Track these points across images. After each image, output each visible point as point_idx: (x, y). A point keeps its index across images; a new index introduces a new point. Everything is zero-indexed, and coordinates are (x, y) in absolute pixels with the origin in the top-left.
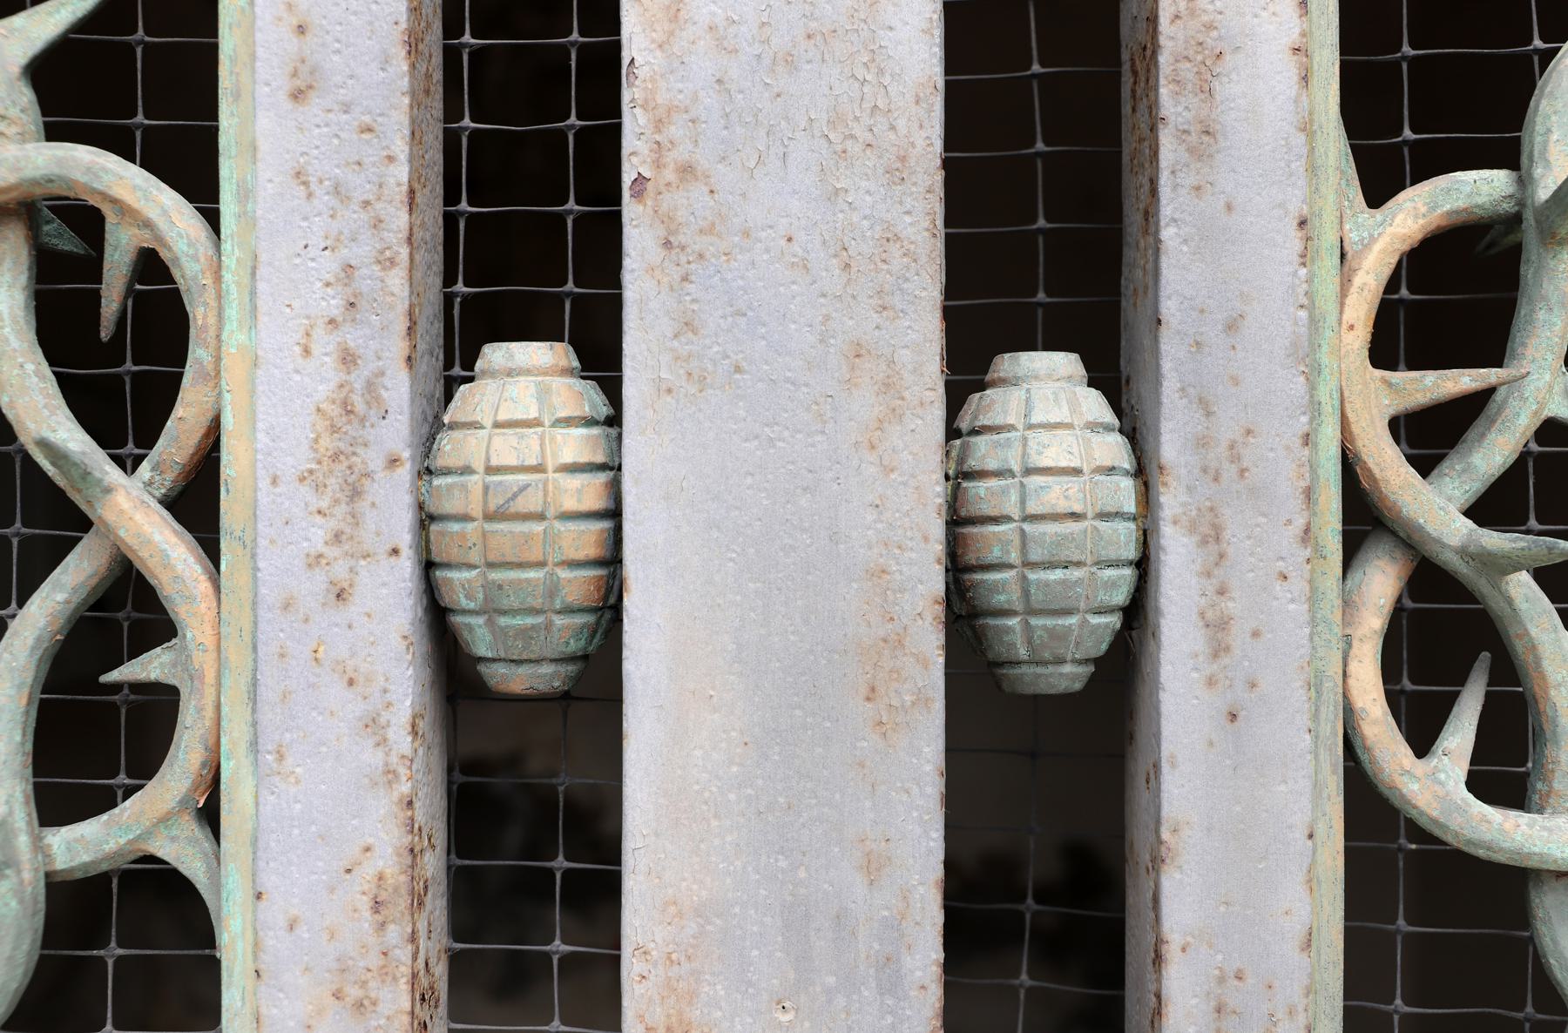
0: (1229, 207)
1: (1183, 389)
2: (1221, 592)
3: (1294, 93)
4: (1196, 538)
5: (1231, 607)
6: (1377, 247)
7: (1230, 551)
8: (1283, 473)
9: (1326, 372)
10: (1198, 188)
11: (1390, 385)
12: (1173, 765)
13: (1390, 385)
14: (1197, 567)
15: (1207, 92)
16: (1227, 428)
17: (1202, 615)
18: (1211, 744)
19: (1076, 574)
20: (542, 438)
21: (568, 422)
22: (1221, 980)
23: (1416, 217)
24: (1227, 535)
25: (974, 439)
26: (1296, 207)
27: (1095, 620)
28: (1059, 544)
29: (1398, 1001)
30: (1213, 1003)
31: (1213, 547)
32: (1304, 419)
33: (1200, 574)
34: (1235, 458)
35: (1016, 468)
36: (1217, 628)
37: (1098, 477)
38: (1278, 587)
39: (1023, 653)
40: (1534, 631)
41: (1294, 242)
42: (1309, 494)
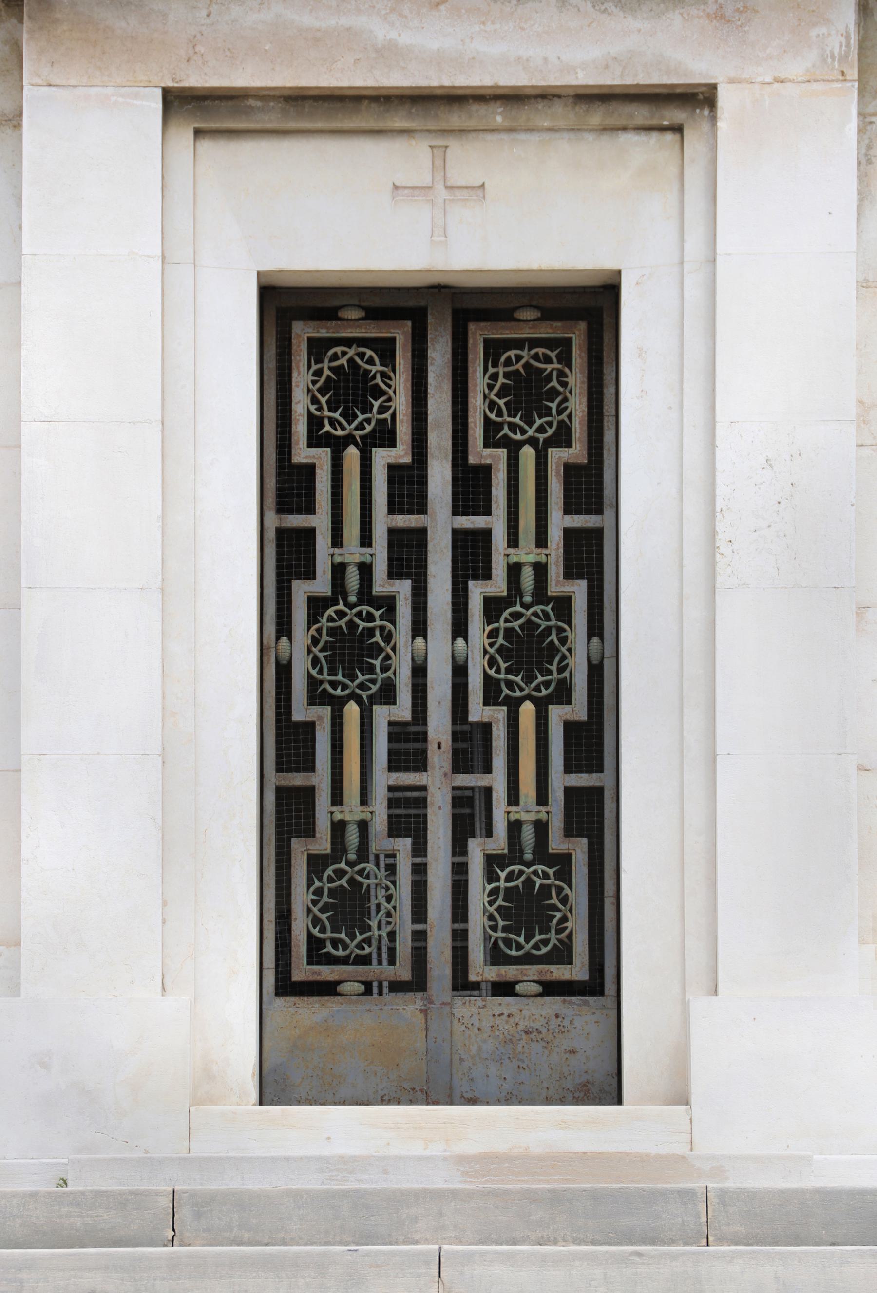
8: (478, 646)
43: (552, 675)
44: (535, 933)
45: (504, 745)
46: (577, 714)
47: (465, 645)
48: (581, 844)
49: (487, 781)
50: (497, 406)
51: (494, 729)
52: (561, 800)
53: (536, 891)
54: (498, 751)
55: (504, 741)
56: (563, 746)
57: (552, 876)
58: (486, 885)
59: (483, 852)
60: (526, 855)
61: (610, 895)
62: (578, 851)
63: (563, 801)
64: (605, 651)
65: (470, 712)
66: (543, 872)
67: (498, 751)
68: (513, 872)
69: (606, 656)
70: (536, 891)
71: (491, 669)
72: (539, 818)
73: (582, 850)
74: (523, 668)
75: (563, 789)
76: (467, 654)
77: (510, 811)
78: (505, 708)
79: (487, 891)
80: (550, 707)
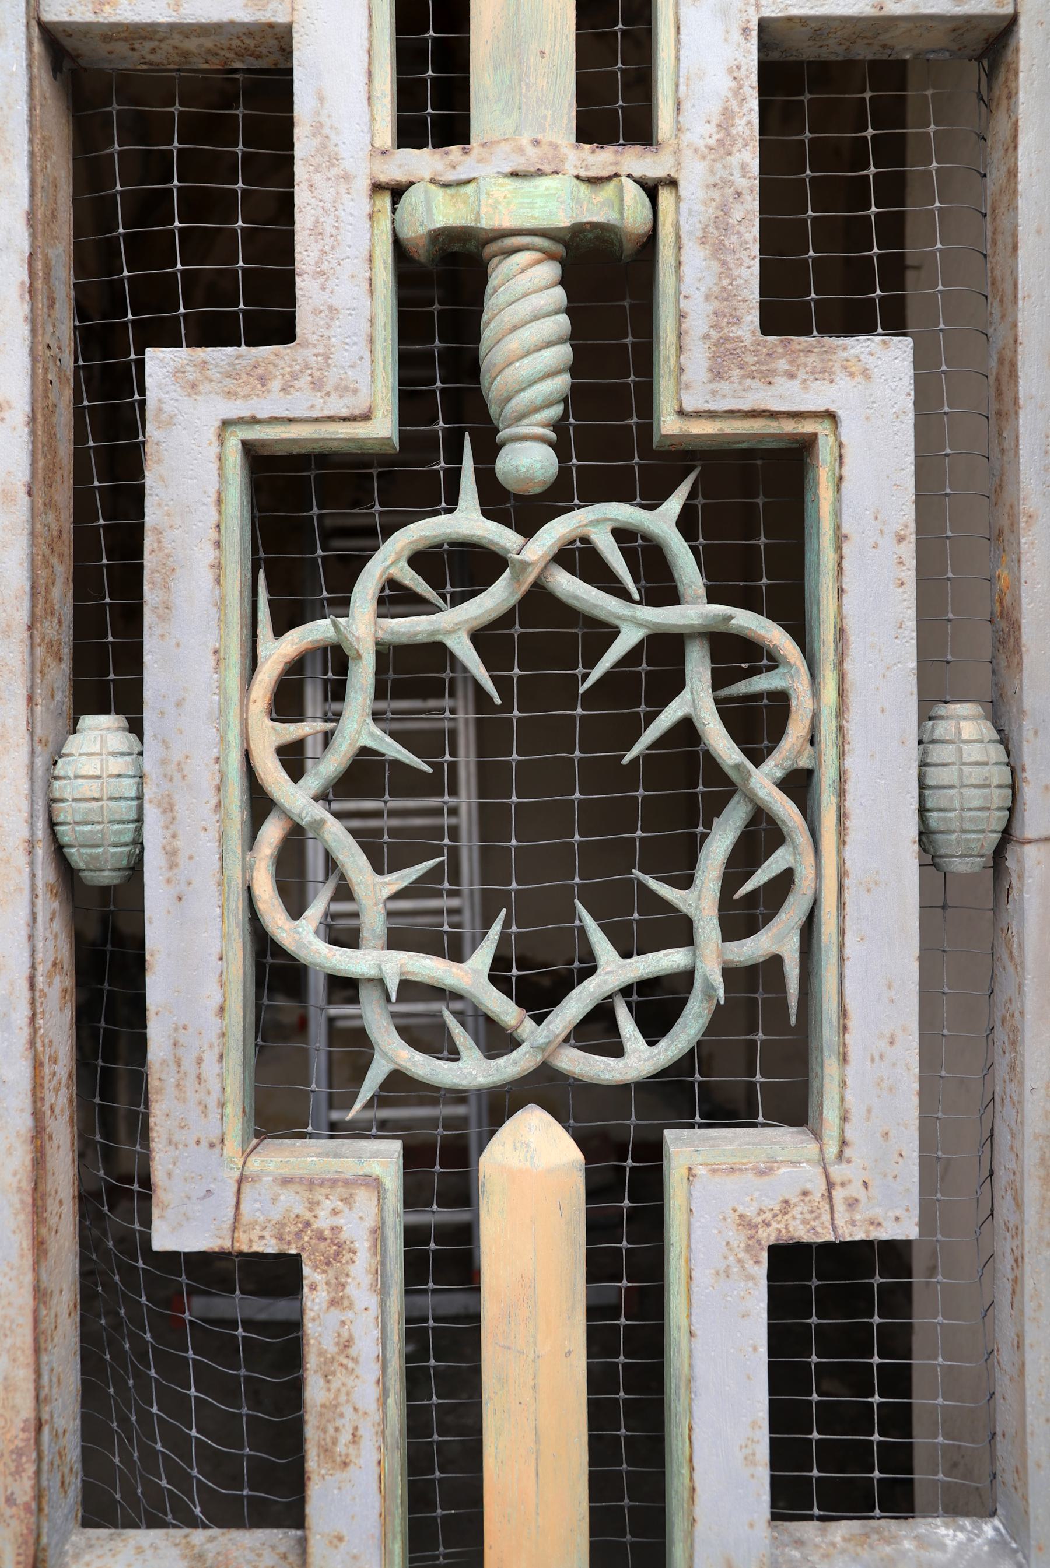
0: (178, 645)
1: (155, 736)
2: (174, 836)
3: (210, 587)
4: (160, 810)
5: (179, 843)
6: (270, 661)
7: (178, 816)
8: (204, 777)
9: (232, 725)
10: (162, 636)
11: (274, 729)
12: (150, 923)
13: (274, 729)
14: (162, 824)
15: (166, 587)
16: (177, 756)
17: (164, 848)
18: (169, 912)
19: (98, 827)
20: (102, 760)
21: (113, 754)
22: (176, 1029)
23: (292, 644)
24: (176, 808)
25: (931, 746)
26: (214, 644)
27: (991, 835)
28: (87, 813)
30: (172, 1041)
31: (169, 814)
32: (215, 750)
33: (163, 828)
34: (180, 770)
35: (72, 775)
36: (171, 854)
37: (111, 780)
38: (202, 834)
41: (211, 661)
46: (852, 1204)
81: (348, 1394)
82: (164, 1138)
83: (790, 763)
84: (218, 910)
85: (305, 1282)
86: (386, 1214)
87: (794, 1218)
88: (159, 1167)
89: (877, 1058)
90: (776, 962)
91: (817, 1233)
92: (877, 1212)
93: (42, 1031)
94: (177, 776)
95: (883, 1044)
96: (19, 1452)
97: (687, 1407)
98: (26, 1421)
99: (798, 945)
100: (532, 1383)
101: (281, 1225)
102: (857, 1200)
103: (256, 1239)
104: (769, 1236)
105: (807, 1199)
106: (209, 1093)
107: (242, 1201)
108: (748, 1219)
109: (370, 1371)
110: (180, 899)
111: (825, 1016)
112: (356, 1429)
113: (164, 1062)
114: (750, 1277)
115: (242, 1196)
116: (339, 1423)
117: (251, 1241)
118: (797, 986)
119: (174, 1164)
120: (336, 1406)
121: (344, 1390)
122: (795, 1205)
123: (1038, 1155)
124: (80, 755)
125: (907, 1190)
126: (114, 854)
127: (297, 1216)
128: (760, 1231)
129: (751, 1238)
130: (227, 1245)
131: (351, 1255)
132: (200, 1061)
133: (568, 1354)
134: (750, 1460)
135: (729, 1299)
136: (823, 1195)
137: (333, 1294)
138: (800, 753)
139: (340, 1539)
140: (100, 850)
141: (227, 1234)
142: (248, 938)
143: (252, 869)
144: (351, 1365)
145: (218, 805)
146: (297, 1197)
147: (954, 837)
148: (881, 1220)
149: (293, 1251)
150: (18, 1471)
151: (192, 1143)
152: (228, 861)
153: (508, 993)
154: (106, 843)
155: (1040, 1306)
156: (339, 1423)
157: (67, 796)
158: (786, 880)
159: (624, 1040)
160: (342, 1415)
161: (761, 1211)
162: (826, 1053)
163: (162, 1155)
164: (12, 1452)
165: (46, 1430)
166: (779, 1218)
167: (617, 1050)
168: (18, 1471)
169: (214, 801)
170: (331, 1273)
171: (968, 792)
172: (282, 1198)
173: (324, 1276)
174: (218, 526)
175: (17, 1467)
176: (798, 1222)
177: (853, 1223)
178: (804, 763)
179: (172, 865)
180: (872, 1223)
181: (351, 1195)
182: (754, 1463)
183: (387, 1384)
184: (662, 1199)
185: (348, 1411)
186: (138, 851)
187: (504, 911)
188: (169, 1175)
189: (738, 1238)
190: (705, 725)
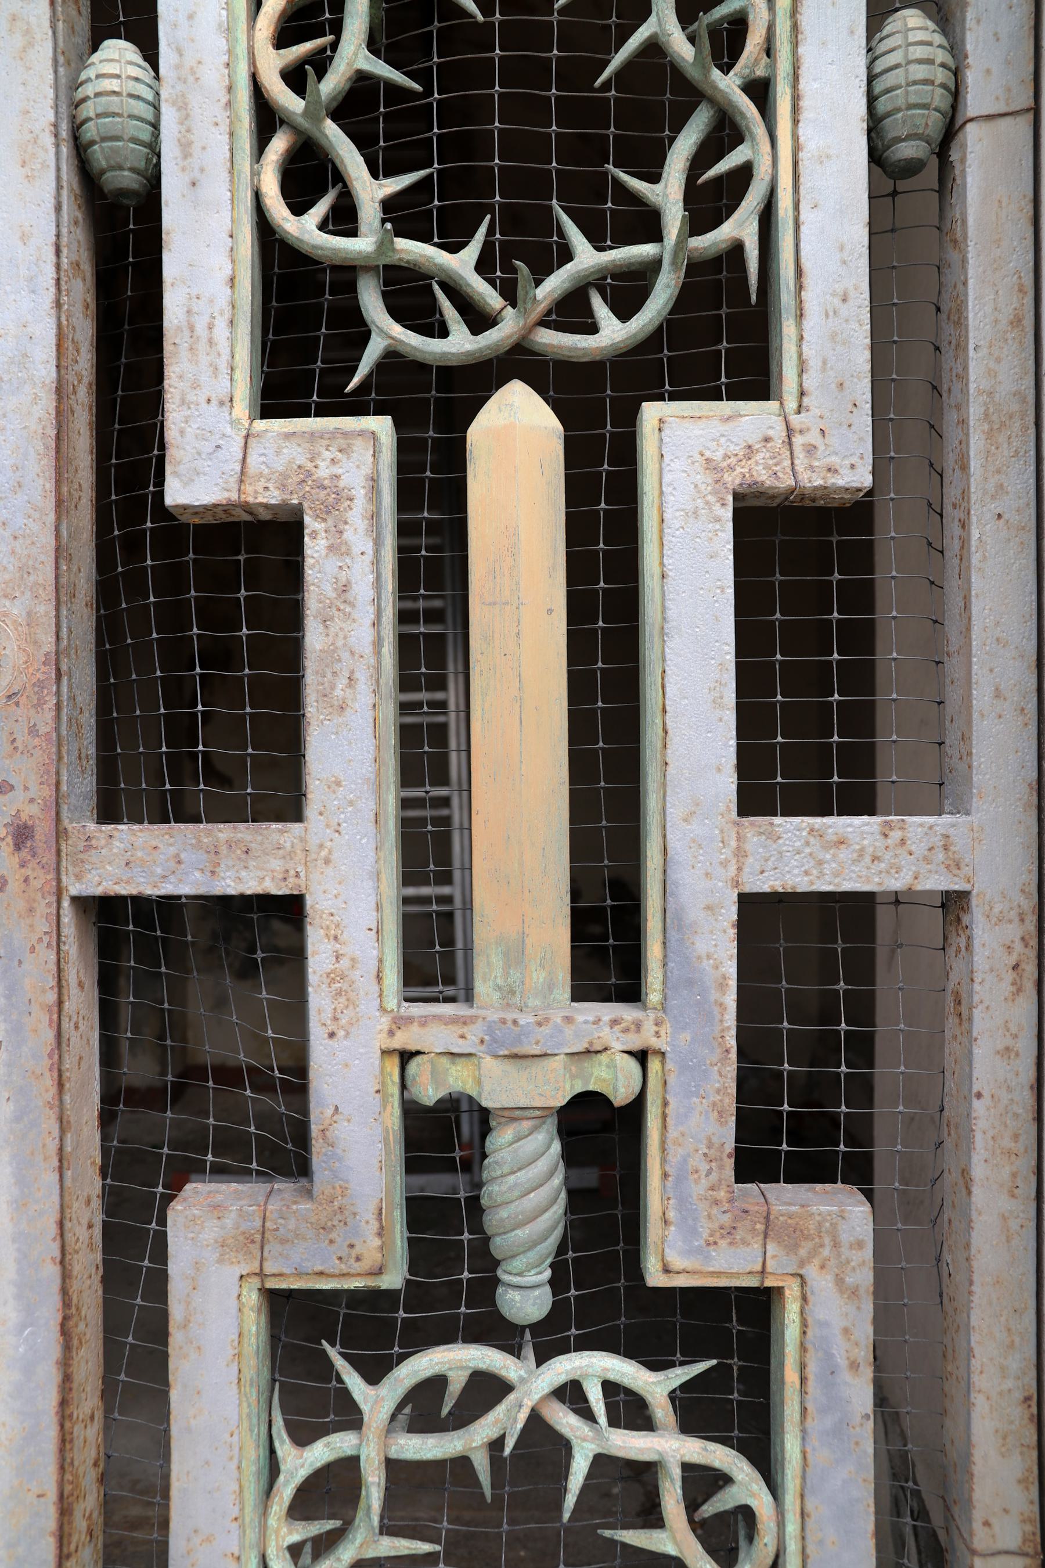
7: (191, 113)
8: (213, 77)
12: (167, 205)
17: (179, 140)
19: (118, 119)
29: (784, 983)
31: (184, 112)
38: (213, 129)
39: (104, 164)
40: (341, 152)
42: (230, 89)
43: (655, 234)
44: (671, 1365)
45: (378, 643)
46: (811, 450)
47: (144, 73)
48: (836, 1245)
49: (276, 864)
50: (338, 1523)
51: (315, 548)
52: (722, 986)
53: (570, 1500)
54: (341, 683)
55: (376, 624)
56: (730, 648)
57: (662, 1410)
58: (285, 1448)
59: (255, 1283)
60: (514, 1296)
61: (1000, 1545)
62: (821, 1282)
63: (733, 983)
64: (971, 77)
65: (172, 454)
66: (610, 1388)
67: (341, 683)
68: (436, 1384)
69: (974, 103)
70: (570, 1500)
71: (298, 209)
72: (591, 1087)
73: (839, 1281)
74: (489, 208)
75: (732, 913)
76: (156, 126)
77: (413, 1047)
78: (382, 426)
79: (286, 1490)
80: (651, 412)
81: (345, 638)
82: (177, 400)
83: (748, 71)
84: (229, 194)
85: (306, 531)
86: (381, 467)
87: (757, 463)
88: (173, 426)
89: (831, 313)
90: (737, 249)
91: (778, 478)
92: (834, 460)
93: (66, 307)
94: (191, 79)
95: (837, 301)
96: (40, 684)
97: (660, 655)
98: (47, 654)
99: (757, 228)
100: (516, 631)
101: (285, 476)
102: (815, 447)
103: (261, 490)
104: (733, 480)
105: (769, 445)
106: (219, 355)
107: (248, 455)
108: (714, 464)
109: (365, 615)
110: (194, 184)
111: (782, 282)
112: (352, 672)
113: (179, 329)
114: (718, 520)
115: (249, 451)
116: (337, 667)
117: (256, 492)
118: (756, 266)
119: (187, 422)
120: (334, 651)
121: (341, 635)
122: (757, 451)
123: (983, 409)
124: (101, 62)
125: (861, 439)
126: (133, 150)
127: (299, 467)
128: (726, 475)
129: (717, 482)
130: (234, 496)
131: (349, 502)
132: (211, 327)
133: (550, 611)
134: (718, 703)
135: (698, 540)
136: (783, 442)
137: (332, 541)
138: (757, 61)
139: (338, 784)
140: (120, 144)
141: (235, 486)
142: (255, 231)
143: (259, 174)
144: (348, 609)
145: (229, 104)
146: (300, 450)
147: (900, 115)
148: (838, 467)
149: (295, 502)
150: (39, 705)
151: (202, 400)
152: (237, 158)
153: (495, 287)
154: (126, 137)
155: (985, 557)
156: (337, 667)
157: (92, 114)
158: (744, 174)
159: (598, 319)
160: (339, 660)
161: (726, 456)
162: (784, 316)
163: (174, 414)
164: (34, 685)
165: (65, 680)
166: (743, 463)
167: (593, 329)
168: (39, 705)
169: (224, 100)
170: (330, 522)
171: (913, 67)
172: (285, 451)
173: (323, 525)
174: (232, 322)
175: (39, 699)
176: (761, 467)
177: (811, 468)
178: (760, 72)
179: (186, 155)
180: (829, 470)
181: (349, 445)
182: (722, 707)
183: (382, 634)
184: (635, 464)
185: (345, 656)
186: (155, 161)
187: (488, 217)
188: (182, 432)
189: (703, 479)
190: (670, 35)
